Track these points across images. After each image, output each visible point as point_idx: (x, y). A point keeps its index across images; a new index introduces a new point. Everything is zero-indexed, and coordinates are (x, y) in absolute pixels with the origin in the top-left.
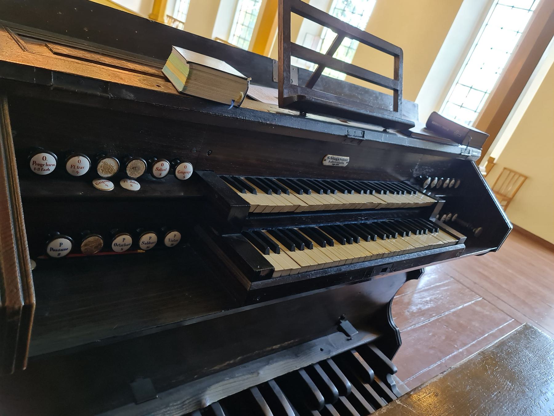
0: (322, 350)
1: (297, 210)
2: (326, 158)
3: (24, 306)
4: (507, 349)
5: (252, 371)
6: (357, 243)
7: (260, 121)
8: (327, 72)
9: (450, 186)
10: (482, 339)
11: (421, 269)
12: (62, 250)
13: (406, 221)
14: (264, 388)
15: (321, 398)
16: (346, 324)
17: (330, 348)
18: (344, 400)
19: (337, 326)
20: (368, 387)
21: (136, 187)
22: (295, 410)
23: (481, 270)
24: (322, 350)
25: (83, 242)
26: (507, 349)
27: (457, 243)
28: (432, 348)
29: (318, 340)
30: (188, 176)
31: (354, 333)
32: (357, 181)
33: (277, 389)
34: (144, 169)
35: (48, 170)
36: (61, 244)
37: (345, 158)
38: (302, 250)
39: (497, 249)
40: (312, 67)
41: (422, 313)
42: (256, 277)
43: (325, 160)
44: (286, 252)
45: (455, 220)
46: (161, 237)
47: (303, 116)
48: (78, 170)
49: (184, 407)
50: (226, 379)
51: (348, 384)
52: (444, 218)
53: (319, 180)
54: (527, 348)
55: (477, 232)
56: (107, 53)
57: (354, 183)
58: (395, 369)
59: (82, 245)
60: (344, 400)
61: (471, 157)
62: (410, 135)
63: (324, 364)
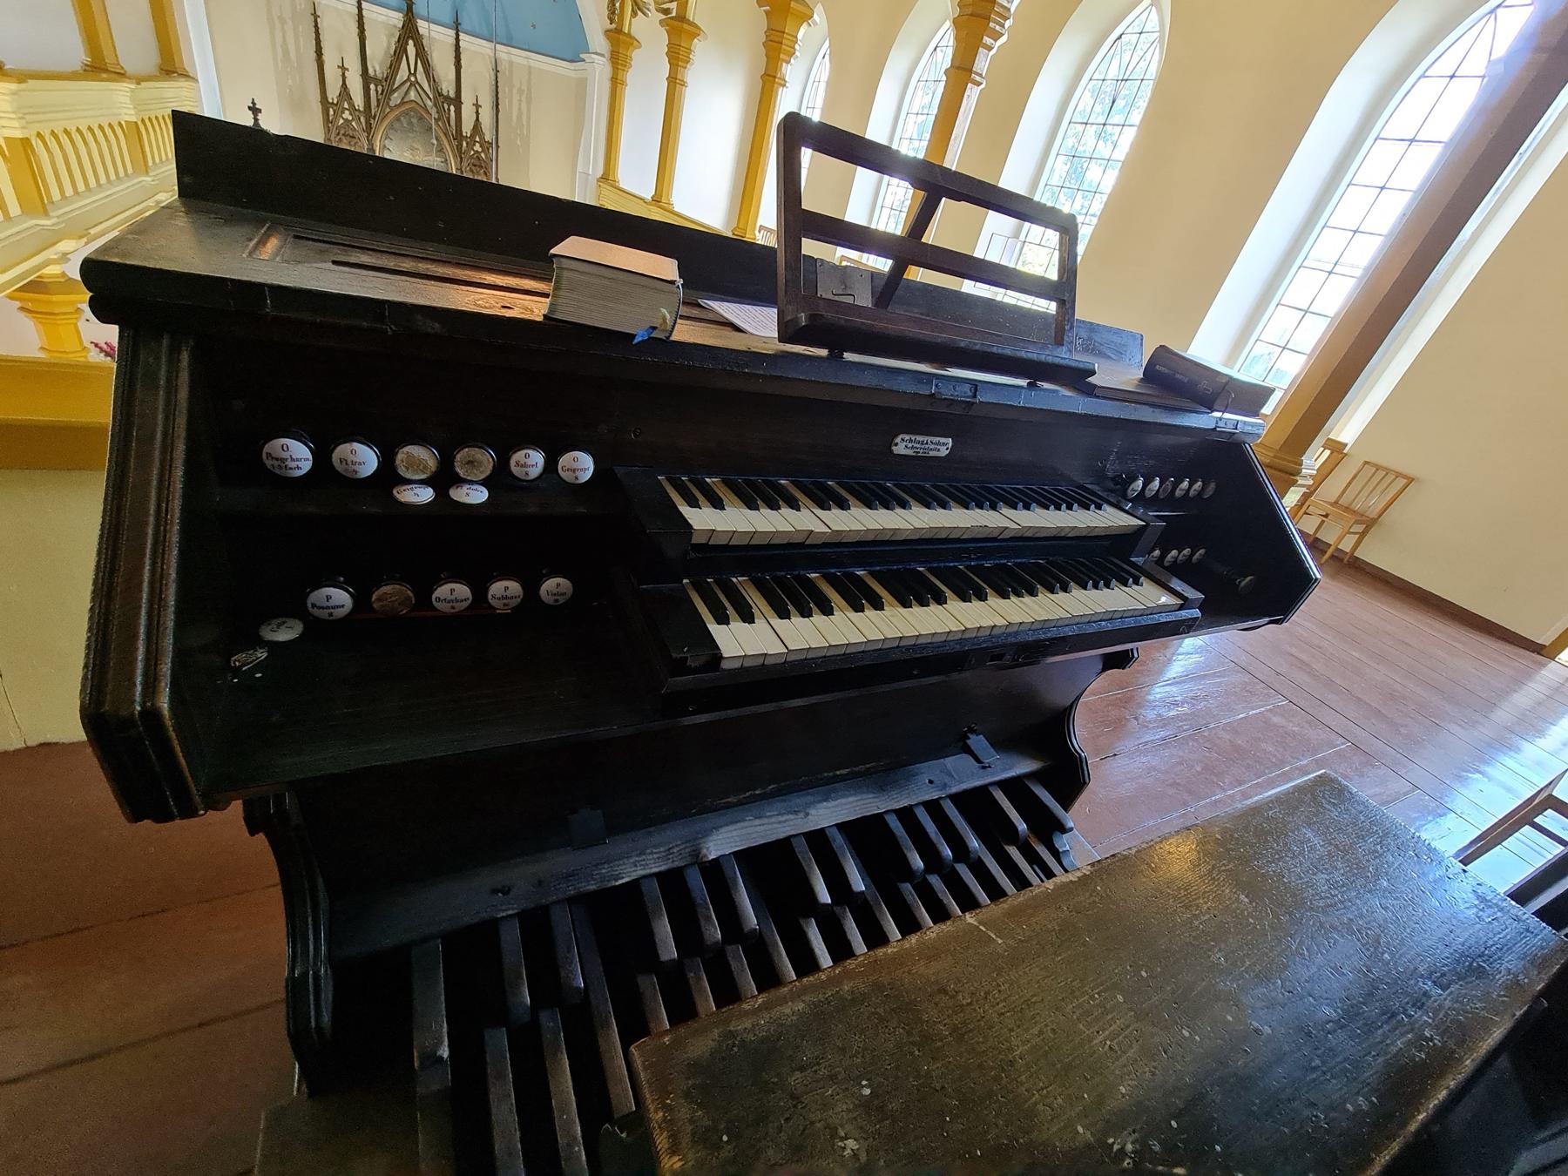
0: (931, 782)
1: (809, 539)
2: (898, 440)
3: (140, 712)
4: (1261, 825)
5: (796, 809)
6: (941, 605)
7: (728, 368)
8: (917, 274)
9: (1192, 493)
10: (1278, 776)
11: (1132, 650)
12: (334, 607)
13: (1073, 562)
14: (817, 839)
15: (917, 862)
16: (977, 742)
17: (947, 780)
18: (935, 881)
19: (961, 744)
20: (1013, 851)
21: (477, 495)
22: (867, 879)
23: (1294, 651)
24: (931, 782)
25: (374, 592)
26: (1261, 825)
27: (1181, 608)
28: (1174, 784)
29: (926, 764)
30: (586, 476)
31: (991, 756)
32: (1046, 487)
33: (838, 841)
34: (492, 464)
35: (299, 468)
36: (329, 598)
37: (943, 440)
38: (808, 617)
39: (1285, 619)
40: (884, 265)
41: (1164, 722)
42: (680, 667)
43: (896, 444)
44: (769, 620)
45: (1199, 561)
46: (531, 588)
47: (836, 355)
48: (353, 467)
49: (671, 856)
50: (747, 818)
51: (974, 843)
52: (1172, 557)
53: (1046, 487)
54: (1309, 825)
55: (1243, 584)
56: (519, 270)
57: (965, 489)
58: (1070, 824)
59: (373, 599)
60: (935, 881)
61: (1243, 436)
62: (1091, 391)
63: (933, 807)
